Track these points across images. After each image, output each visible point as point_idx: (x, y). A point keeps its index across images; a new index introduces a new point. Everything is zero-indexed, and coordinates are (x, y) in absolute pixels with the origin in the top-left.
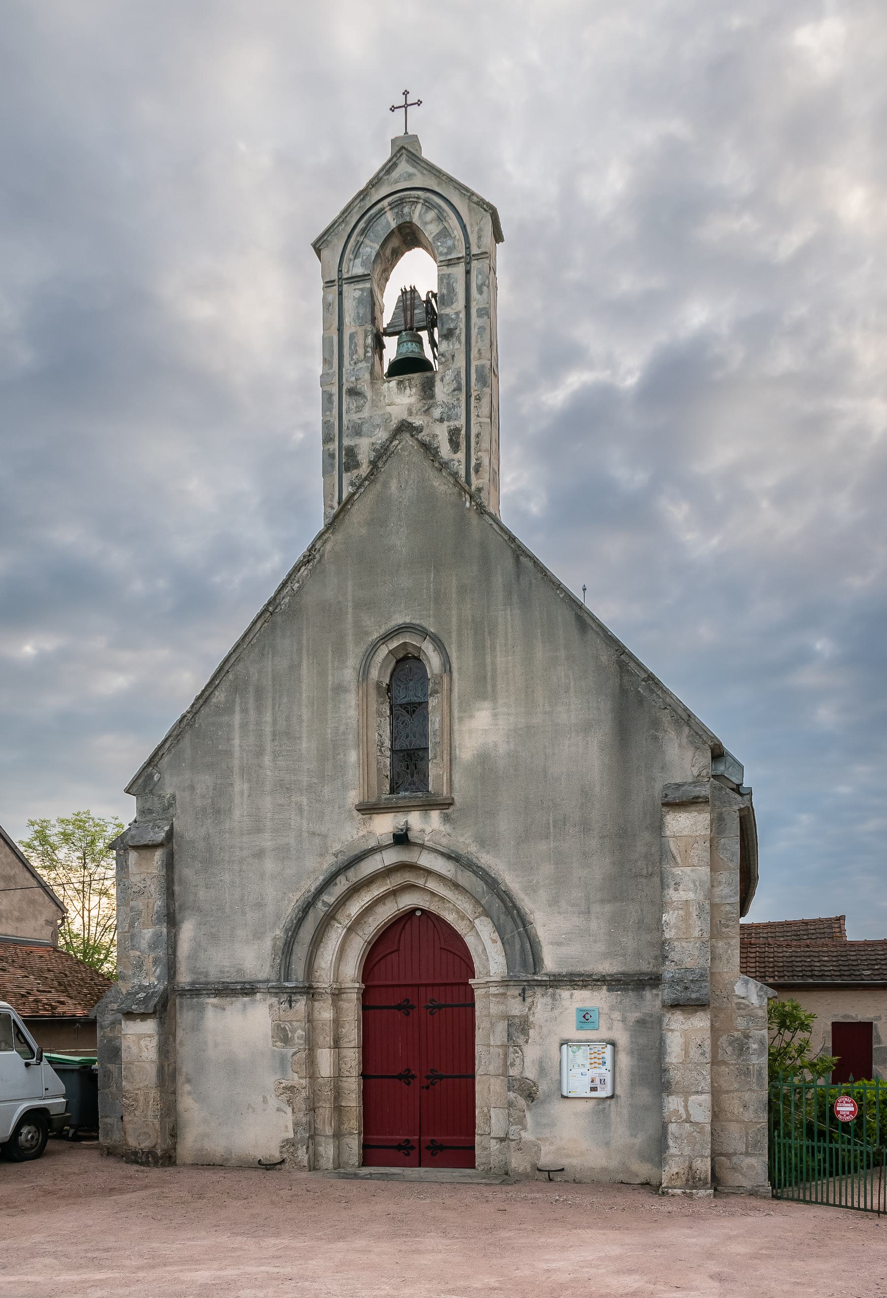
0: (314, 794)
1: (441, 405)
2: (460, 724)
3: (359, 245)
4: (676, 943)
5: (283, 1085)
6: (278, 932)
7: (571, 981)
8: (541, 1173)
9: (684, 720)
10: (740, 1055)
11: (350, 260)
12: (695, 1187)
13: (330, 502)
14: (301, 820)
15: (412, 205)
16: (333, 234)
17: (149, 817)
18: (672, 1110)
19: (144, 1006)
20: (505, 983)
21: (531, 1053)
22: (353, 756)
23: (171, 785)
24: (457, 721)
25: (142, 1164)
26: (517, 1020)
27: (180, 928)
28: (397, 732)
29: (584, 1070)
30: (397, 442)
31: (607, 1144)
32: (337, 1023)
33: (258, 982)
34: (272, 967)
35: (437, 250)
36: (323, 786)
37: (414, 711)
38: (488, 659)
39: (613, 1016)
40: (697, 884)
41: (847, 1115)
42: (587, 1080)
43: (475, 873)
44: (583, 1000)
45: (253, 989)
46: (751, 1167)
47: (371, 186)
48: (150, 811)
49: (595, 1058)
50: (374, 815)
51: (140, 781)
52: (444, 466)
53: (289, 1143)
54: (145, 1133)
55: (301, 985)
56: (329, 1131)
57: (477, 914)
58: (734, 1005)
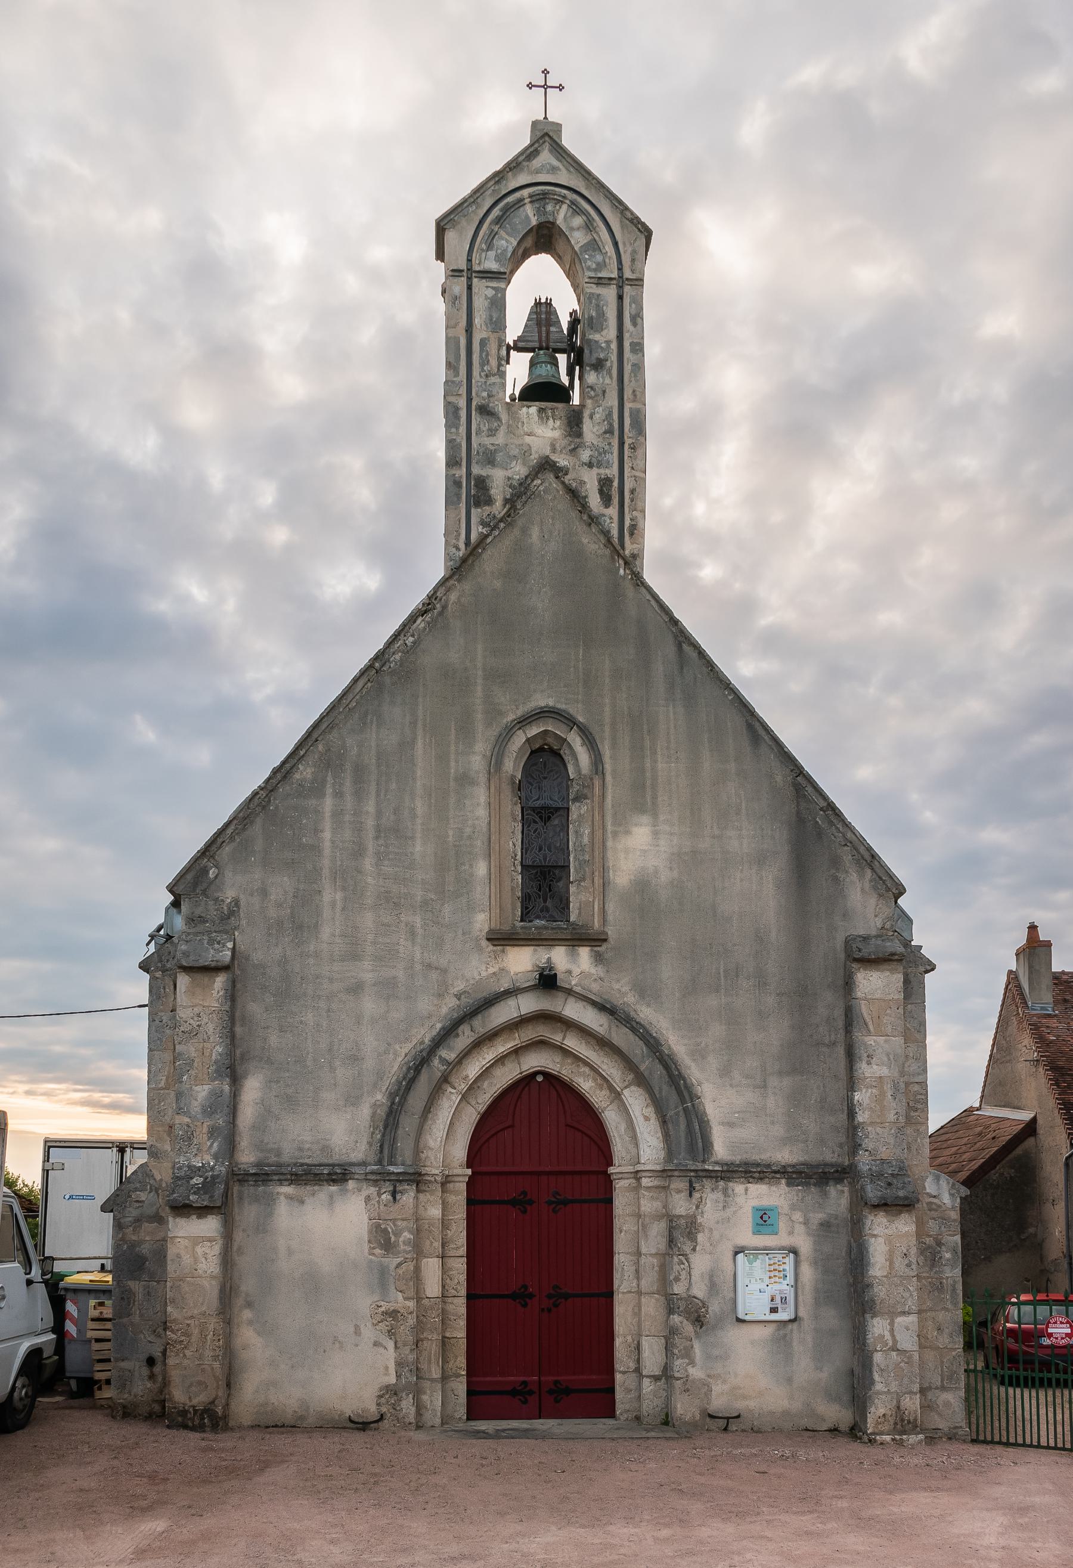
1: (590, 447)
2: (614, 839)
3: (492, 235)
4: (870, 1129)
5: (383, 1309)
6: (379, 1096)
7: (746, 1172)
8: (713, 1420)
9: (866, 861)
10: (933, 1266)
11: (483, 250)
12: (903, 1432)
13: (454, 541)
15: (556, 204)
16: (461, 214)
17: (200, 928)
18: (877, 1335)
19: (207, 1196)
20: (664, 1174)
21: (700, 1263)
22: (481, 869)
23: (233, 885)
24: (610, 836)
25: (193, 1429)
27: (241, 1086)
28: (529, 842)
29: (763, 1286)
30: (539, 482)
31: (789, 1380)
32: (445, 1224)
33: (350, 1165)
34: (370, 1144)
35: (585, 263)
36: (443, 905)
37: (549, 818)
38: (648, 765)
39: (794, 1218)
40: (891, 1057)
41: (1062, 1338)
42: (766, 1298)
43: (633, 1030)
44: (759, 1197)
46: (947, 1404)
47: (508, 169)
48: (202, 920)
49: (775, 1270)
50: (508, 947)
51: (189, 877)
52: (593, 520)
53: (391, 1391)
54: (200, 1383)
56: (436, 1373)
58: (925, 1205)
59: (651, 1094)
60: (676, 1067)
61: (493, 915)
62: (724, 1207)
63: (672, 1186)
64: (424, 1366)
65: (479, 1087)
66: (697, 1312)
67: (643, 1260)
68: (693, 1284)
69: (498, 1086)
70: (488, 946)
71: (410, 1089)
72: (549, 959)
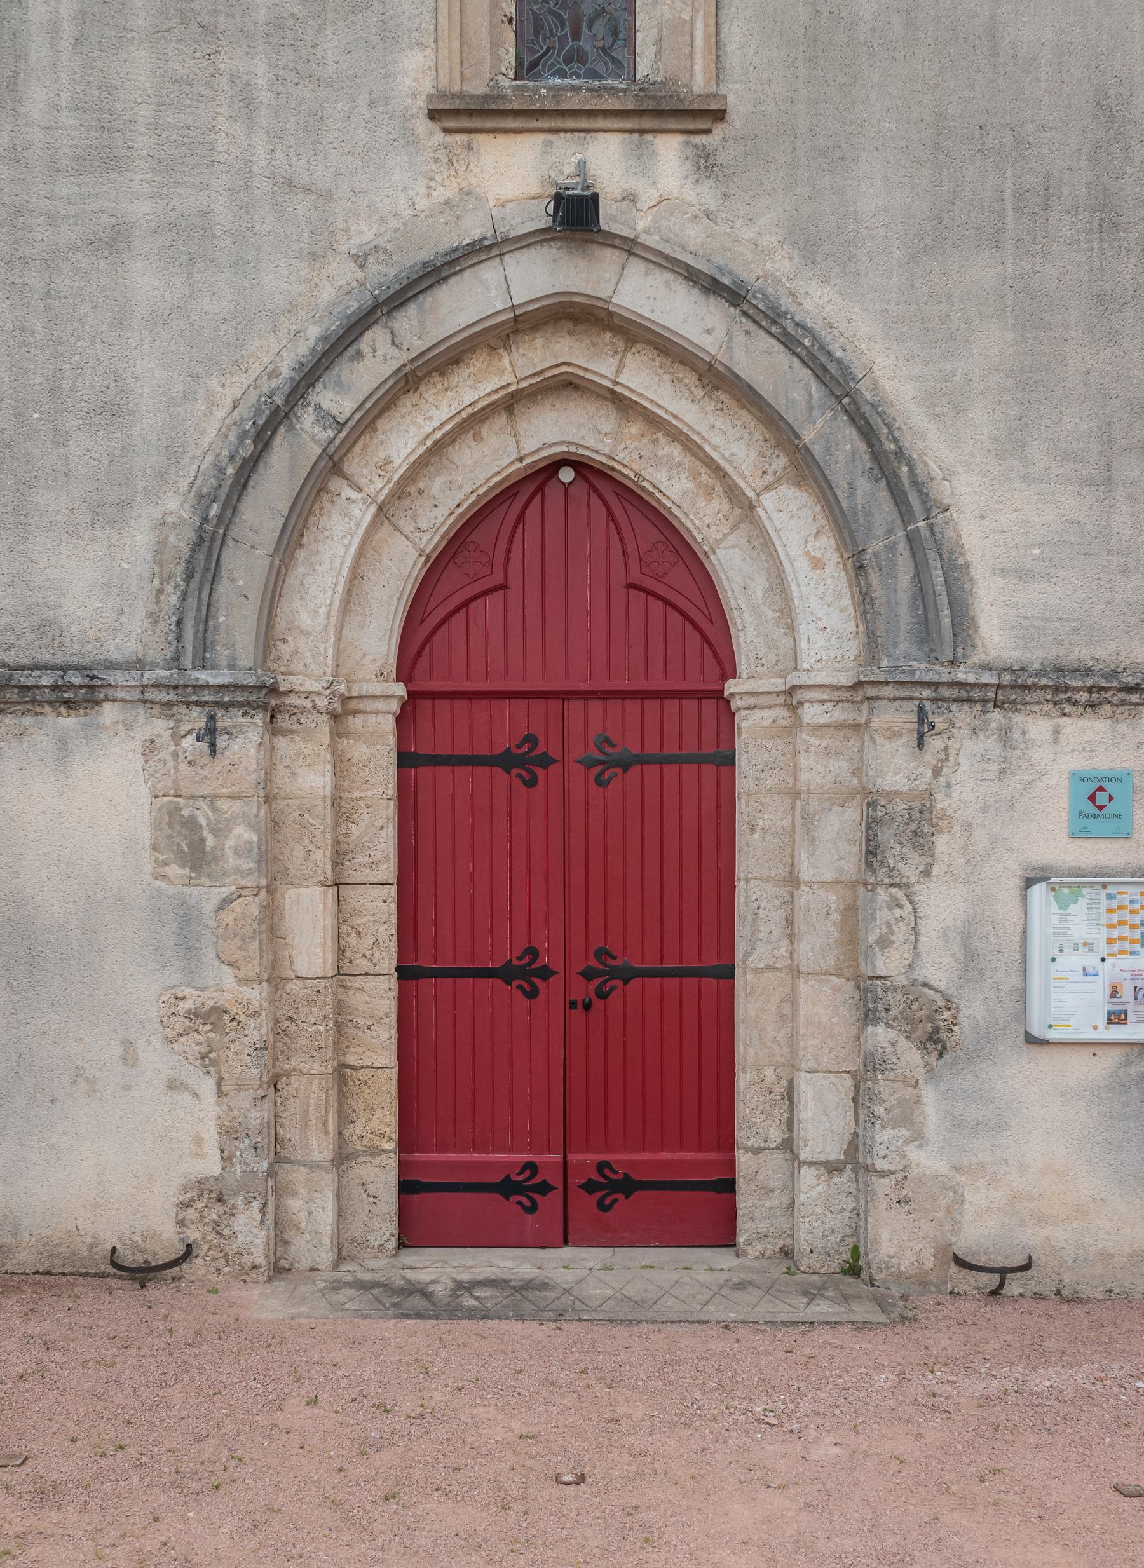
0: (290, 51)
5: (188, 1005)
6: (173, 503)
7: (1056, 689)
8: (965, 1271)
14: (249, 136)
26: (900, 806)
29: (1092, 961)
34: (154, 617)
36: (321, 29)
42: (1099, 988)
43: (788, 341)
45: (91, 688)
50: (480, 138)
55: (251, 680)
56: (321, 1148)
57: (770, 478)
59: (828, 503)
60: (890, 431)
61: (444, 53)
62: (1002, 771)
63: (876, 723)
64: (290, 1132)
65: (421, 492)
66: (931, 1019)
67: (804, 896)
68: (924, 953)
69: (467, 489)
70: (431, 134)
71: (245, 486)
72: (582, 166)
